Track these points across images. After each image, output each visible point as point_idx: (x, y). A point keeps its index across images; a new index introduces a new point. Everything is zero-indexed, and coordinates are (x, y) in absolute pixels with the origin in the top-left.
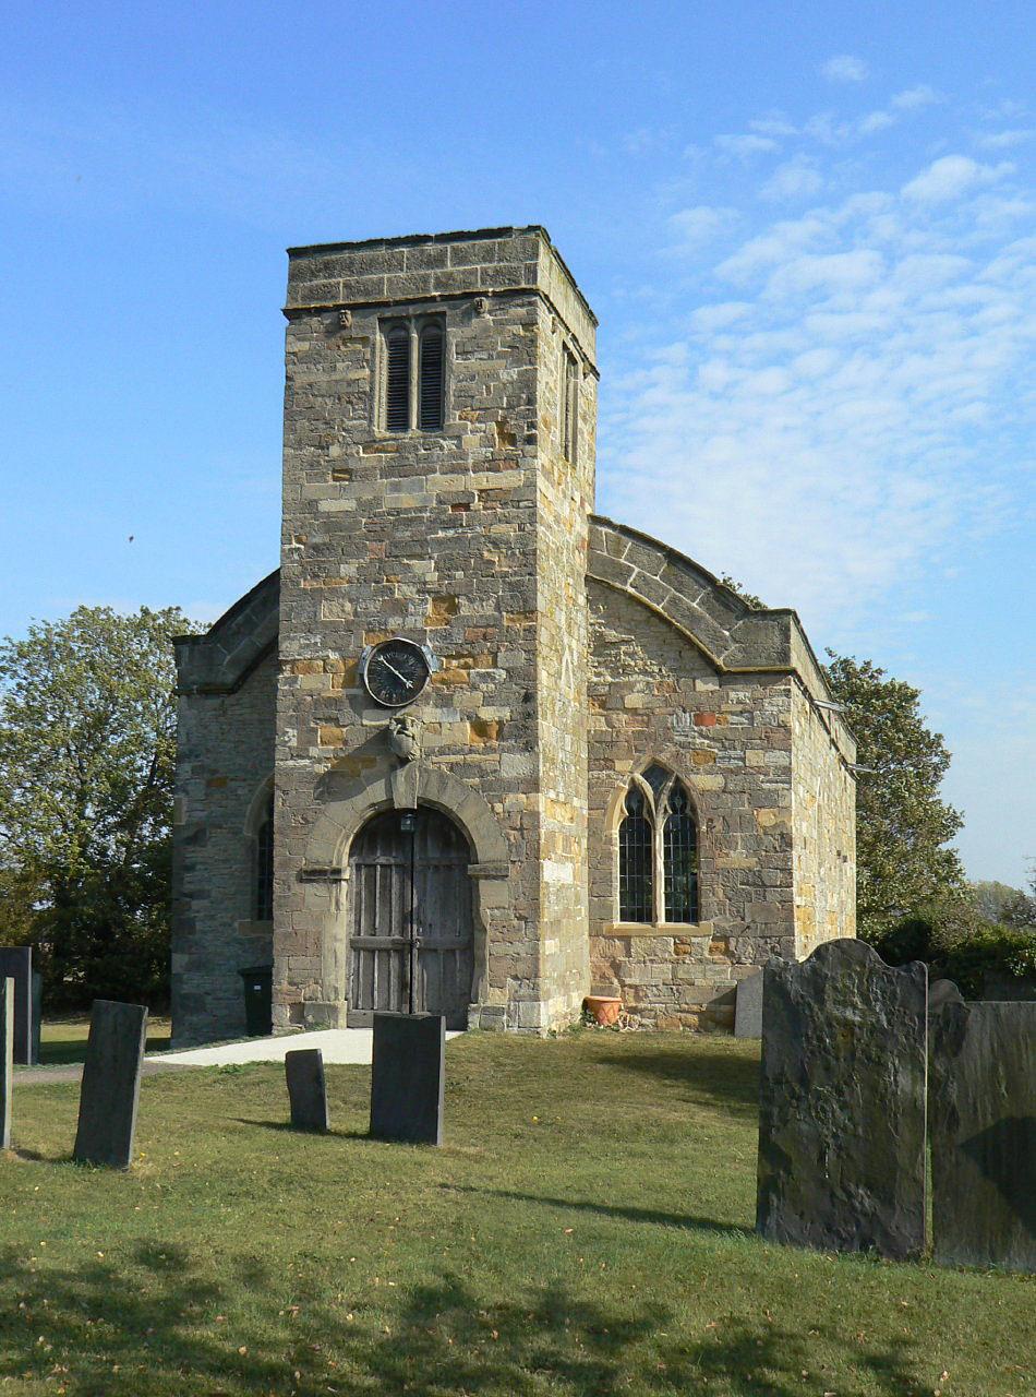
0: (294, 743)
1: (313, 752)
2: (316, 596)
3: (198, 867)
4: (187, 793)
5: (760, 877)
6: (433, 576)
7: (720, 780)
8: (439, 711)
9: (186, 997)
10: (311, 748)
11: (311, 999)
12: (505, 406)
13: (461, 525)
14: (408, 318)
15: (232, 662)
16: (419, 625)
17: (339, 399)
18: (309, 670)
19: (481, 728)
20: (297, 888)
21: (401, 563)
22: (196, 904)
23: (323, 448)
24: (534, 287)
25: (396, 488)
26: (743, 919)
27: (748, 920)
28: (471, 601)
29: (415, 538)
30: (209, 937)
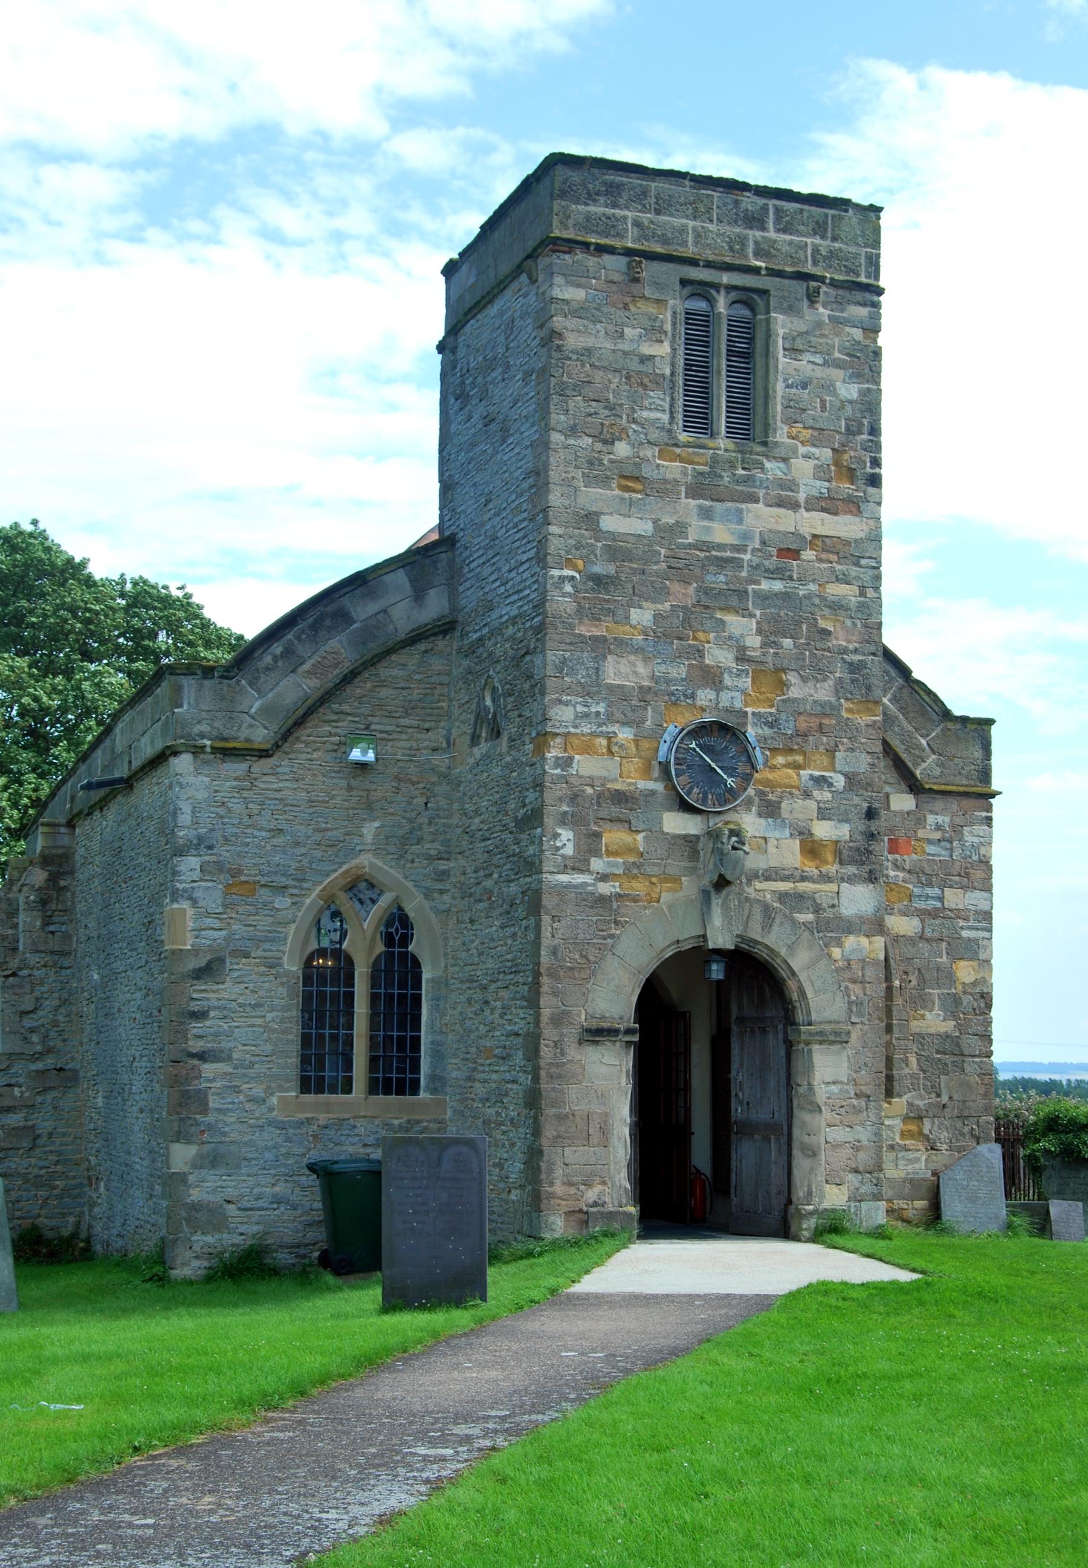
0: (569, 850)
1: (597, 864)
2: (601, 647)
3: (212, 1014)
4: (194, 902)
5: (958, 1045)
6: (754, 641)
7: (915, 922)
8: (762, 821)
9: (196, 1207)
10: (593, 860)
11: (595, 1204)
12: (843, 430)
13: (791, 578)
14: (717, 287)
15: (267, 711)
16: (738, 705)
17: (628, 378)
18: (588, 749)
19: (812, 848)
20: (573, 1052)
21: (712, 617)
22: (209, 1069)
23: (605, 442)
24: (875, 283)
25: (707, 514)
26: (939, 1096)
27: (945, 1099)
28: (804, 680)
29: (732, 587)
30: (231, 1118)
